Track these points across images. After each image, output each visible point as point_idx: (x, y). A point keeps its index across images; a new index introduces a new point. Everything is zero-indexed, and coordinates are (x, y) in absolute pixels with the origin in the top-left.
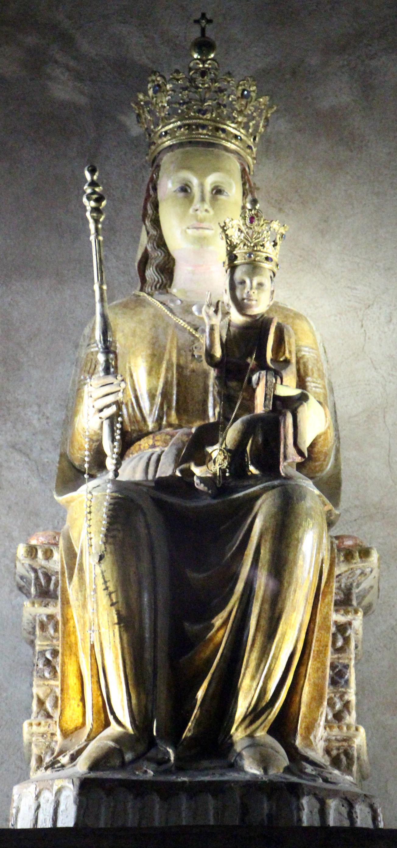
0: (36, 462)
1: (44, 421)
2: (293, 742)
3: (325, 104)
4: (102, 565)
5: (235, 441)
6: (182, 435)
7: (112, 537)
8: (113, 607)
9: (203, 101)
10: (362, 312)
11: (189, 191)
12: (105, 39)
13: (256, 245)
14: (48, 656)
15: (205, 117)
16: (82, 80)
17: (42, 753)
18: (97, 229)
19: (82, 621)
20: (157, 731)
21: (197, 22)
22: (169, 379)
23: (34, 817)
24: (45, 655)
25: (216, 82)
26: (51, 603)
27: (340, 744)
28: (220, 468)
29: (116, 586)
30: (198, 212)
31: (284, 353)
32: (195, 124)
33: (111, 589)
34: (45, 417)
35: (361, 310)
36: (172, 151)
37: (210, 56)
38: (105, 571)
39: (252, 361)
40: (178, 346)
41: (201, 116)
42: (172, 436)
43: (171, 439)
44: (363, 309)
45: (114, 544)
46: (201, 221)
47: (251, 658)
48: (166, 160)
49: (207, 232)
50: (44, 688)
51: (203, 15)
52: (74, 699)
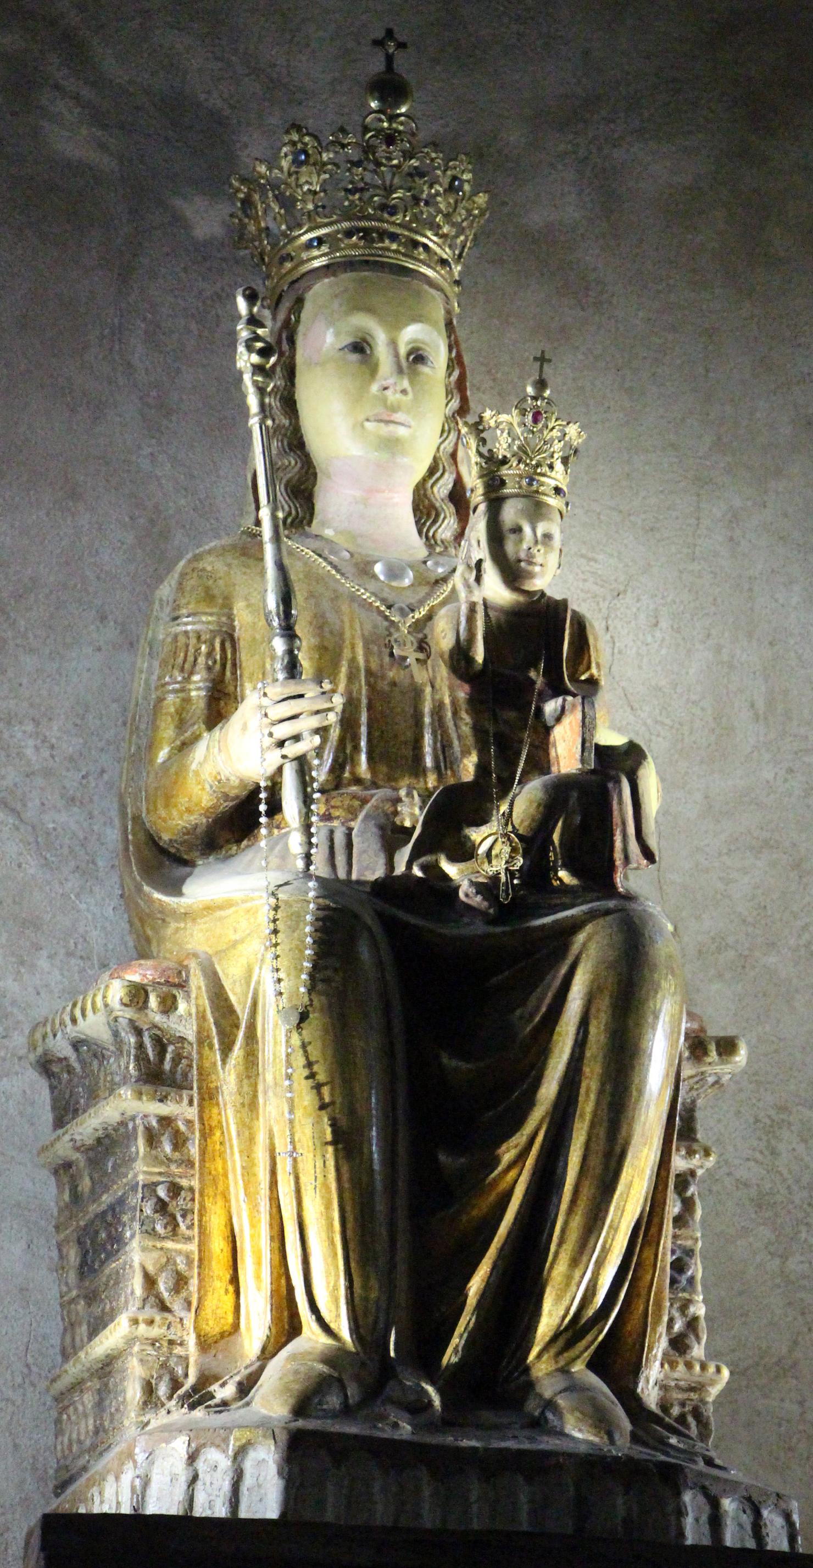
0: (33, 827)
1: (46, 753)
2: (631, 1386)
3: (537, 218)
4: (304, 1032)
5: (533, 820)
6: (382, 801)
7: (323, 981)
8: (323, 1112)
9: (389, 190)
10: (607, 603)
11: (368, 352)
12: (146, 55)
13: (538, 465)
14: (162, 1192)
15: (394, 218)
16: (104, 127)
17: (152, 1377)
18: (262, 405)
19: (247, 1133)
20: (395, 1350)
21: (378, 43)
22: (355, 694)
23: (187, 1497)
24: (155, 1191)
25: (411, 158)
26: (172, 1094)
27: (685, 1396)
28: (507, 869)
29: (331, 1074)
30: (389, 393)
31: (589, 668)
32: (377, 230)
33: (321, 1077)
34: (46, 744)
35: (604, 600)
36: (334, 275)
37: (399, 108)
38: (310, 1043)
39: (537, 677)
40: (363, 635)
41: (386, 215)
42: (364, 801)
43: (362, 807)
44: (609, 598)
45: (327, 995)
46: (394, 409)
47: (566, 1223)
48: (319, 291)
49: (401, 431)
50: (155, 1255)
51: (390, 33)
52: (220, 1278)
